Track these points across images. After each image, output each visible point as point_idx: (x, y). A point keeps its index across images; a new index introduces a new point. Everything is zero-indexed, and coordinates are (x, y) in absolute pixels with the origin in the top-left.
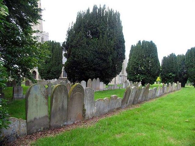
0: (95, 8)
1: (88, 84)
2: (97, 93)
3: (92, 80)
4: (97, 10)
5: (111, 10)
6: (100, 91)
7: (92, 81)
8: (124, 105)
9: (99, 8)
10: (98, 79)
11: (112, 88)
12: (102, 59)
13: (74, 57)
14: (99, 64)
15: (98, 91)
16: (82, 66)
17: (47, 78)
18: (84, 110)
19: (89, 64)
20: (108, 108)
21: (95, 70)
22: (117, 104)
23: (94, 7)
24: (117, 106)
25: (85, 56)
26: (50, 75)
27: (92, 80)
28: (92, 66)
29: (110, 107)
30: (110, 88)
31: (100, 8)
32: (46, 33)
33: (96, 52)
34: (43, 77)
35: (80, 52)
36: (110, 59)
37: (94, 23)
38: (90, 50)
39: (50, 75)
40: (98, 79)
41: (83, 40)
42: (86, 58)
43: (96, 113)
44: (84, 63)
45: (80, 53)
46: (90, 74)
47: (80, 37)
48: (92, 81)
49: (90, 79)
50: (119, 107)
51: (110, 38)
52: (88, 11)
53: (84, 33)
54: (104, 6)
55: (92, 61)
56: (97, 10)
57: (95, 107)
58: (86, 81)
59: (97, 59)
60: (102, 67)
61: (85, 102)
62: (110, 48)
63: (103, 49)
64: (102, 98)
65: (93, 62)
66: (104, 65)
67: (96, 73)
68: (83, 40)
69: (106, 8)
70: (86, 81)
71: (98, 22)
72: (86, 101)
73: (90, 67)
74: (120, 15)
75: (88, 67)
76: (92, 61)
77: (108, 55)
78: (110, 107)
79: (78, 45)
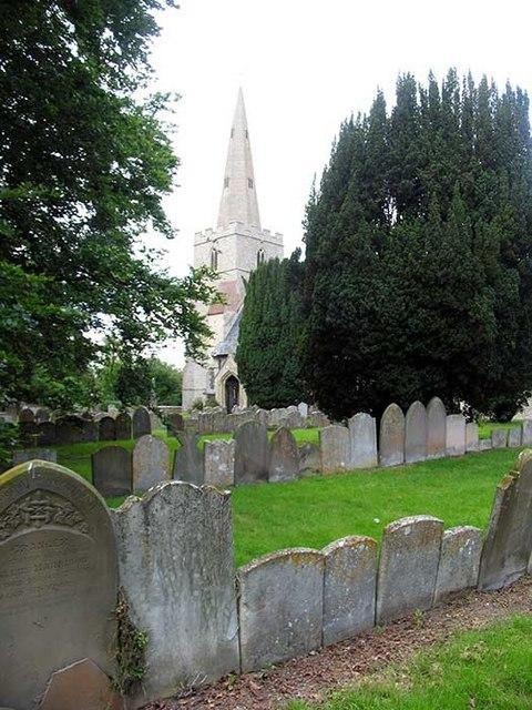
0: (406, 88)
1: (384, 427)
2: (424, 469)
3: (405, 411)
4: (418, 95)
5: (484, 81)
6: (448, 457)
7: (405, 413)
8: (508, 571)
9: (426, 86)
10: (436, 401)
11: (511, 440)
12: (446, 311)
13: (324, 308)
14: (437, 331)
15: (437, 456)
16: (356, 348)
17: (272, 400)
18: (128, 643)
19: (389, 337)
20: (366, 601)
21: (417, 360)
22: (445, 569)
23: (400, 83)
24: (446, 578)
25: (367, 304)
26: (282, 391)
27: (405, 411)
28: (399, 347)
29: (381, 594)
30: (500, 442)
31: (433, 85)
32: (273, 234)
33: (418, 279)
34: (256, 398)
35: (344, 286)
36: (485, 308)
37: (403, 154)
38: (391, 273)
39: (282, 391)
40: (436, 401)
41: (355, 230)
42: (372, 312)
43: (253, 645)
44: (364, 335)
45: (345, 291)
46: (394, 382)
47: (346, 223)
48: (405, 413)
49: (394, 406)
50: (464, 583)
51: (482, 210)
52: (379, 104)
53: (362, 201)
54: (452, 74)
55: (403, 324)
56: (418, 95)
57: (243, 609)
58: (378, 414)
59: (422, 312)
60: (451, 346)
61: (147, 582)
62: (482, 257)
63: (448, 263)
64: (307, 539)
65: (407, 326)
66: (459, 337)
67: (423, 378)
68: (355, 230)
69: (460, 81)
70: (378, 414)
71: (420, 148)
72: (156, 577)
73: (396, 352)
74: (527, 103)
75: (385, 350)
76: (403, 324)
77: (474, 288)
78: (387, 595)
79: (336, 255)
